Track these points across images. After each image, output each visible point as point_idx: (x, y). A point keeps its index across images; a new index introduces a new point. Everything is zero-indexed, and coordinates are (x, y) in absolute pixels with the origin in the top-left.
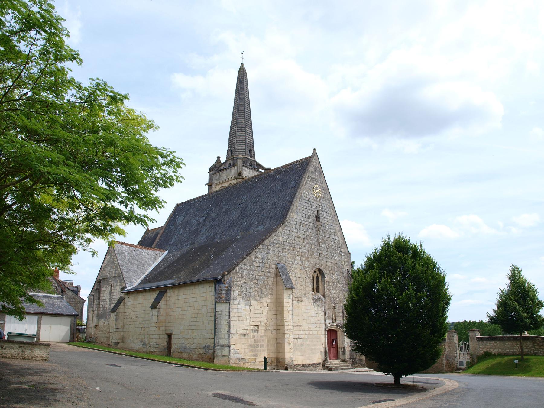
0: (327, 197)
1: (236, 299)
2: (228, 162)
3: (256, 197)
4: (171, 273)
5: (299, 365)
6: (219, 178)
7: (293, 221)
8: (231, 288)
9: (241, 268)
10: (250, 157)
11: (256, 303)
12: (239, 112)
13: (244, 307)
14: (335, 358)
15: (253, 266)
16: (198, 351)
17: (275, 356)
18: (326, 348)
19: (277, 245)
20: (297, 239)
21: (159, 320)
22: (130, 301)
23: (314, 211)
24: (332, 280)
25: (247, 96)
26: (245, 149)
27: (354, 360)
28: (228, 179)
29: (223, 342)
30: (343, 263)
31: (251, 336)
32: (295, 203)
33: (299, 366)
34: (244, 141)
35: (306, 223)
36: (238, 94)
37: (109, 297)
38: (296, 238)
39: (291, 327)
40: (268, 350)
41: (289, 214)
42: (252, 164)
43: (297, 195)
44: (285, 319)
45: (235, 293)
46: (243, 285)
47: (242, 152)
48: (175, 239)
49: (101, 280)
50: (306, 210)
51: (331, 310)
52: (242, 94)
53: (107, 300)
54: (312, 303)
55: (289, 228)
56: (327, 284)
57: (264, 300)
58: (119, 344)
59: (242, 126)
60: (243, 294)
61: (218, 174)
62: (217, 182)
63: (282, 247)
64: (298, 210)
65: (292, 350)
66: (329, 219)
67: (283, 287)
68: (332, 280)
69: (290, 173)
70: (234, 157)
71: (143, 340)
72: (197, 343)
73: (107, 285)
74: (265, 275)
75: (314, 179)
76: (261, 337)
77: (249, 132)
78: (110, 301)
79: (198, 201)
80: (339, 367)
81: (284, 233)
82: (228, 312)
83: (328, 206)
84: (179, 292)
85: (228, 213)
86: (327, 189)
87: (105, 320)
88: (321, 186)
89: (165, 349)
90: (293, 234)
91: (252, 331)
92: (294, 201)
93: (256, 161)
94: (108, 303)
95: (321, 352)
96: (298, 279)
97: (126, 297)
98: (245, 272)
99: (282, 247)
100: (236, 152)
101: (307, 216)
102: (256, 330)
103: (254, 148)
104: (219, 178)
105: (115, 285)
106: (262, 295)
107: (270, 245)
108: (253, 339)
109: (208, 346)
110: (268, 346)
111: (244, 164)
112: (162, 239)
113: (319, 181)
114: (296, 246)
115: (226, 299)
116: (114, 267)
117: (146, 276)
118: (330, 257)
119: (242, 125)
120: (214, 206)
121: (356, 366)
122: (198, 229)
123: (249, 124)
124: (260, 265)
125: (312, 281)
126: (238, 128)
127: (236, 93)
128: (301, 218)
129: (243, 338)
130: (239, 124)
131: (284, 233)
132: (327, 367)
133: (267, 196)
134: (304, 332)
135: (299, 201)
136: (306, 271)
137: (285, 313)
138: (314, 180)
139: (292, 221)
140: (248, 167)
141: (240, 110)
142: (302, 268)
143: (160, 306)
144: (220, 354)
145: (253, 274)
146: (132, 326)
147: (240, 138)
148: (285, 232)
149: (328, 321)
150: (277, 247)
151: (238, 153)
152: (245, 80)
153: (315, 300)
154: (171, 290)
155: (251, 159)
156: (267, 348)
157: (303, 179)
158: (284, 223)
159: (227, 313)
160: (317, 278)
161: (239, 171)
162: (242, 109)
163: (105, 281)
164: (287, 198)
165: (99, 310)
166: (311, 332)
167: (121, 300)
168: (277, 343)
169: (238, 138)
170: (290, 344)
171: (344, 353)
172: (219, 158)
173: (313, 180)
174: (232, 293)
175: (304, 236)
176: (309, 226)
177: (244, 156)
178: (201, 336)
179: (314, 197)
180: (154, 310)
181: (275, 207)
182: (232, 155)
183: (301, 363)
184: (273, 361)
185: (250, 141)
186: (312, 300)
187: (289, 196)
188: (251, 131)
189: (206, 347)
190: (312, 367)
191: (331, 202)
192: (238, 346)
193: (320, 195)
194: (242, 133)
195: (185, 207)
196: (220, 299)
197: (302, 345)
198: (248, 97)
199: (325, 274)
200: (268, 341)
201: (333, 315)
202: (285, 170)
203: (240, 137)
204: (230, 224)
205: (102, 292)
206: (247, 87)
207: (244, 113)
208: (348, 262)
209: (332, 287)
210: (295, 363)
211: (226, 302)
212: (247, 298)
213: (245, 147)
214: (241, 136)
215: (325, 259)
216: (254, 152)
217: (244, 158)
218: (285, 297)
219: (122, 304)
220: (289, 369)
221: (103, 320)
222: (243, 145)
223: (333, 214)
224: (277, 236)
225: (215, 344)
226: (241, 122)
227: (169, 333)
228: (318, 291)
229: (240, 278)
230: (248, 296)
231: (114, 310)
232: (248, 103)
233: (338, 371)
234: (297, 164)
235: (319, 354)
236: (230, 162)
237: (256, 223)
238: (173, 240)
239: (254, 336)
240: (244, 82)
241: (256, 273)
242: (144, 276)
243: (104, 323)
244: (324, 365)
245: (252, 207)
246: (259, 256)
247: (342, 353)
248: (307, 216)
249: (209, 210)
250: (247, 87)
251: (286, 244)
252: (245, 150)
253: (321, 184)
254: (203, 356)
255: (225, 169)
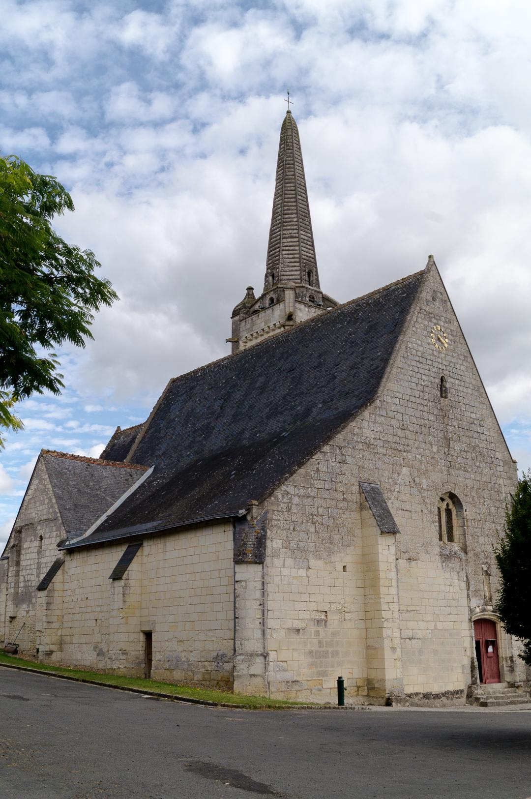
0: (462, 349)
1: (278, 556)
2: (267, 296)
3: (320, 356)
4: (155, 510)
5: (417, 694)
6: (251, 327)
7: (392, 398)
8: (266, 532)
9: (288, 493)
10: (310, 285)
11: (320, 564)
12: (285, 202)
13: (294, 572)
16: (204, 667)
17: (365, 676)
18: (472, 658)
19: (361, 446)
20: (401, 433)
21: (128, 603)
22: (75, 566)
23: (434, 378)
24: (479, 517)
25: (299, 172)
26: (300, 270)
28: (269, 327)
29: (252, 645)
30: (501, 481)
32: (394, 362)
33: (418, 697)
34: (297, 256)
35: (418, 401)
36: (283, 169)
37: (36, 561)
38: (399, 430)
39: (396, 614)
41: (382, 384)
42: (313, 298)
43: (398, 346)
44: (382, 596)
45: (274, 544)
46: (292, 528)
47: (293, 277)
48: (168, 444)
49: (22, 527)
50: (419, 376)
51: (481, 577)
52: (289, 168)
53: (33, 567)
54: (440, 564)
55: (384, 411)
56: (470, 524)
57: (336, 558)
58: (54, 654)
59: (292, 227)
60: (293, 545)
61: (249, 320)
62: (249, 336)
63: (371, 450)
64: (401, 377)
65: (399, 663)
66: (467, 393)
67: (377, 530)
68: (479, 517)
69: (383, 306)
70: (280, 286)
71: (99, 645)
72: (201, 649)
73: (32, 537)
74: (337, 507)
75: (432, 314)
77: (306, 238)
78: (39, 568)
79: (210, 371)
80: (503, 698)
81: (375, 422)
82: (261, 583)
83: (462, 368)
84: (165, 545)
85: (267, 390)
86: (461, 334)
87: (28, 606)
88: (447, 328)
89: (139, 663)
90: (392, 423)
92: (392, 357)
93: (322, 293)
94: (35, 571)
95: (463, 666)
97: (68, 558)
98: (296, 500)
99: (371, 450)
100: (282, 278)
101: (420, 387)
102: (322, 620)
103: (316, 268)
104: (251, 327)
105: (47, 536)
106: (332, 546)
108: (315, 640)
109: (221, 655)
111: (298, 299)
112: (143, 446)
113: (443, 319)
114: (401, 448)
115: (256, 556)
116: (47, 501)
117: (109, 517)
118: (472, 470)
119: (292, 225)
120: (239, 379)
122: (210, 423)
123: (306, 223)
124: (327, 486)
125: (437, 517)
126: (284, 232)
127: (278, 167)
128: (409, 391)
129: (295, 637)
130: (286, 224)
131: (375, 422)
132: (477, 699)
133: (340, 353)
135: (403, 357)
136: (424, 498)
137: (381, 584)
138: (432, 316)
139: (389, 397)
140: (305, 304)
141: (288, 198)
142: (415, 491)
143: (128, 574)
144: (245, 672)
145: (311, 503)
146: (78, 617)
148: (375, 419)
149: (474, 602)
150: (360, 450)
151: (285, 278)
152: (295, 141)
153: (446, 558)
154: (151, 543)
155: (311, 289)
157: (410, 315)
158: (372, 402)
159: (259, 585)
160: (448, 512)
161: (288, 312)
162: (291, 196)
163: (30, 530)
164: (379, 354)
165: (18, 587)
166: (440, 626)
167: (57, 566)
168: (368, 647)
169: (286, 250)
170: (393, 649)
171: (512, 669)
172: (250, 289)
173: (430, 316)
174: (269, 543)
175: (416, 428)
176: (426, 408)
177: (297, 283)
178: (210, 634)
179: (433, 350)
180: (117, 583)
181: (356, 373)
182: (275, 282)
183: (422, 691)
185: (309, 255)
186: (438, 558)
187: (382, 349)
188: (309, 235)
189: (219, 658)
190: (444, 699)
191: (469, 359)
194: (292, 240)
195: (186, 383)
196: (243, 557)
197: (420, 652)
198: (301, 173)
199: (463, 504)
201: (486, 589)
202: (375, 301)
203: (290, 248)
204: (270, 410)
205: (23, 552)
206: (299, 154)
207: (294, 204)
208: (510, 478)
209: (479, 530)
210: (409, 690)
211: (256, 563)
212: (300, 553)
213: (300, 266)
214: (290, 246)
215: (462, 473)
216: (317, 275)
217: (297, 287)
218: (380, 551)
219: (60, 572)
220: (394, 704)
221: (25, 606)
222: (295, 262)
223: (474, 382)
224: (360, 428)
225: (235, 650)
226: (290, 220)
227: (146, 628)
228: (451, 539)
229: (286, 513)
231: (42, 587)
232: (303, 184)
233: (500, 708)
234: (398, 289)
235: (460, 670)
236: (272, 295)
237: (320, 406)
238: (163, 447)
240: (293, 146)
241: (318, 502)
242: (103, 518)
243: (28, 612)
244: (469, 696)
245: (312, 376)
246: (323, 467)
247: (508, 669)
248: (420, 387)
249: (231, 386)
250: (299, 154)
251: (380, 443)
252: (299, 273)
253: (446, 325)
254: (212, 677)
255: (262, 308)
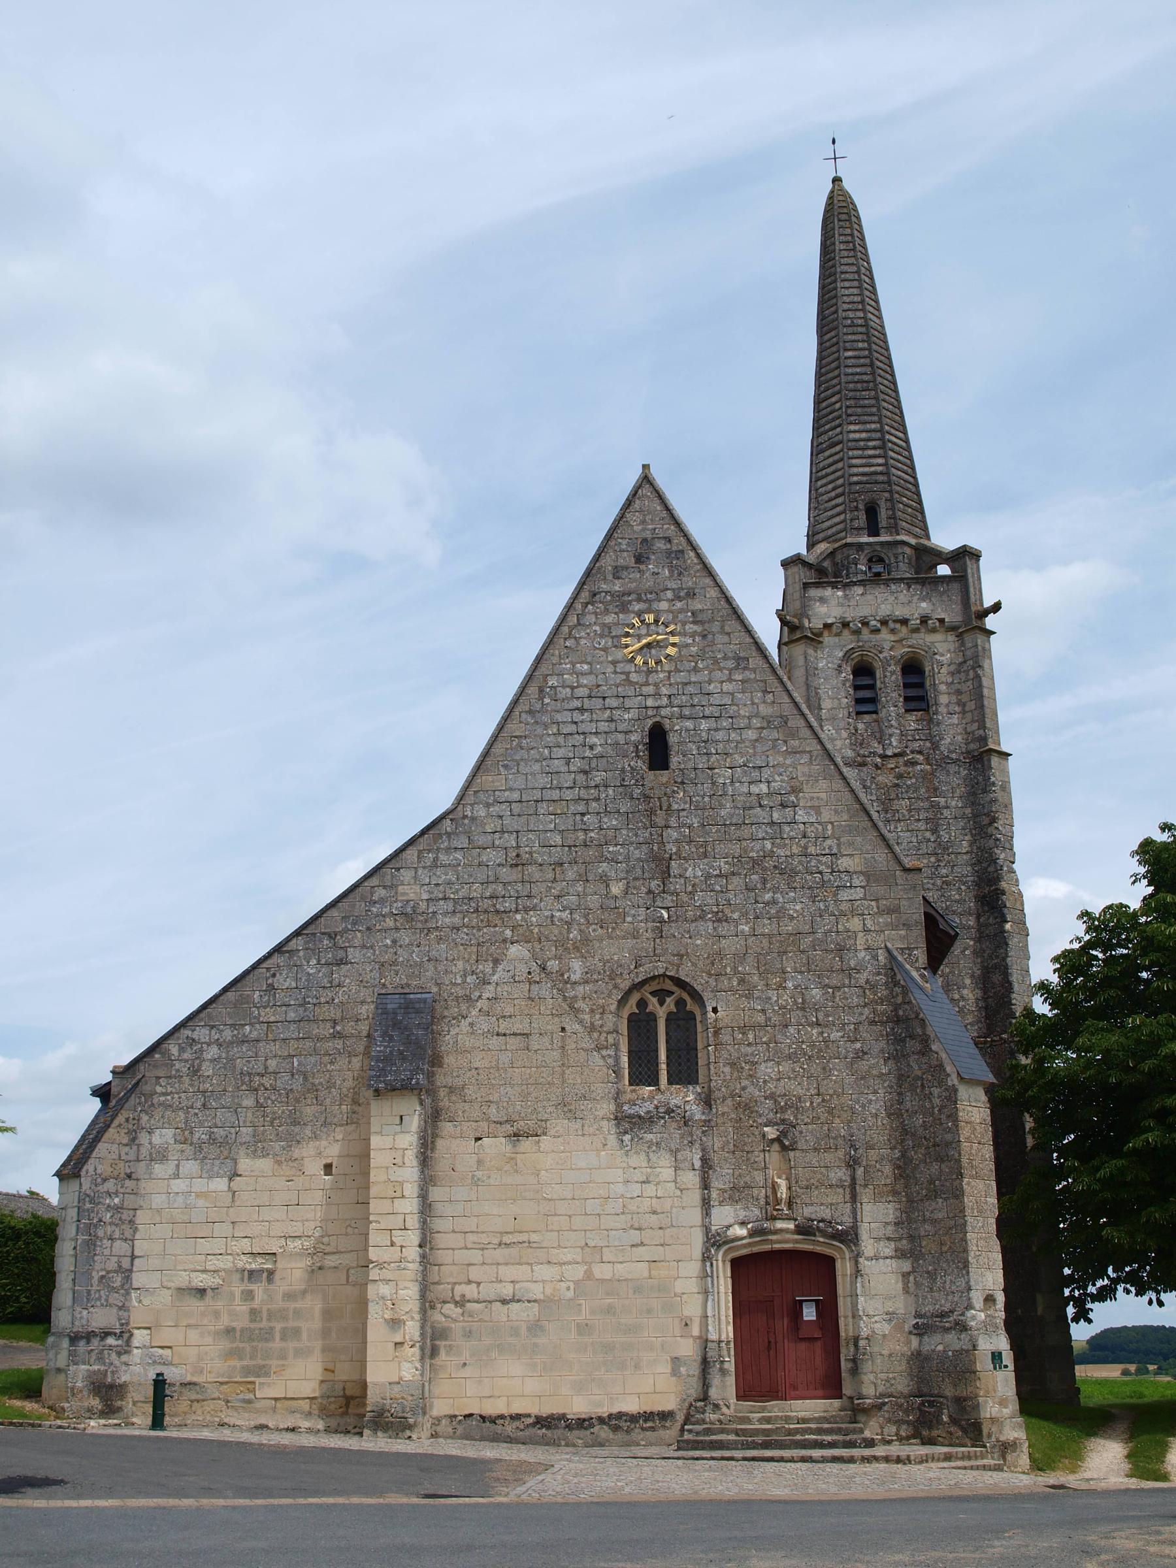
13: (200, 1185)
14: (820, 1392)
19: (390, 923)
27: (931, 1404)
31: (232, 1294)
40: (324, 1350)
46: (199, 1104)
57: (307, 1151)
60: (200, 1134)
76: (289, 1296)
91: (238, 1276)
96: (513, 1042)
106: (297, 1129)
108: (243, 1308)
110: (325, 1333)
121: (935, 1433)
134: (557, 1268)
142: (545, 990)
147: (827, 475)
156: (318, 1345)
166: (602, 1271)
170: (395, 1323)
183: (535, 1410)
184: (353, 1398)
186: (608, 1127)
190: (603, 1432)
192: (167, 1335)
193: (671, 651)
194: (833, 450)
200: (327, 1314)
214: (830, 466)
220: (366, 1432)
229: (186, 1080)
230: (225, 1143)
239: (249, 1295)
247: (850, 1365)
248: (577, 764)
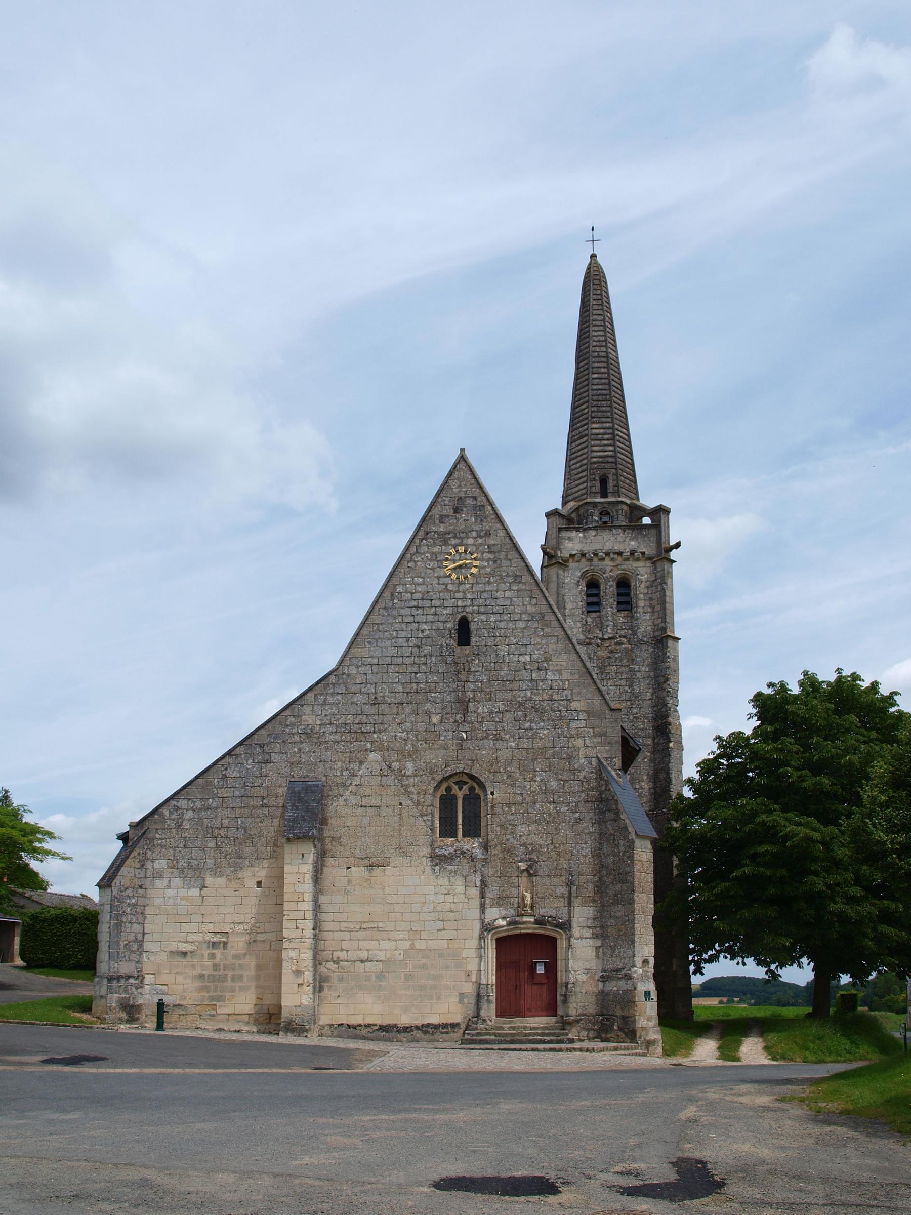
11: (221, 881)
13: (183, 892)
14: (545, 1013)
15: (213, 798)
19: (297, 738)
27: (608, 1019)
40: (257, 987)
46: (181, 845)
60: (182, 863)
63: (315, 740)
76: (236, 957)
106: (240, 861)
107: (270, 743)
108: (209, 963)
110: (258, 978)
134: (393, 943)
147: (577, 457)
156: (253, 984)
166: (420, 945)
186: (426, 862)
190: (418, 1034)
193: (474, 570)
200: (259, 967)
214: (579, 451)
226: (580, 413)
247: (562, 998)
